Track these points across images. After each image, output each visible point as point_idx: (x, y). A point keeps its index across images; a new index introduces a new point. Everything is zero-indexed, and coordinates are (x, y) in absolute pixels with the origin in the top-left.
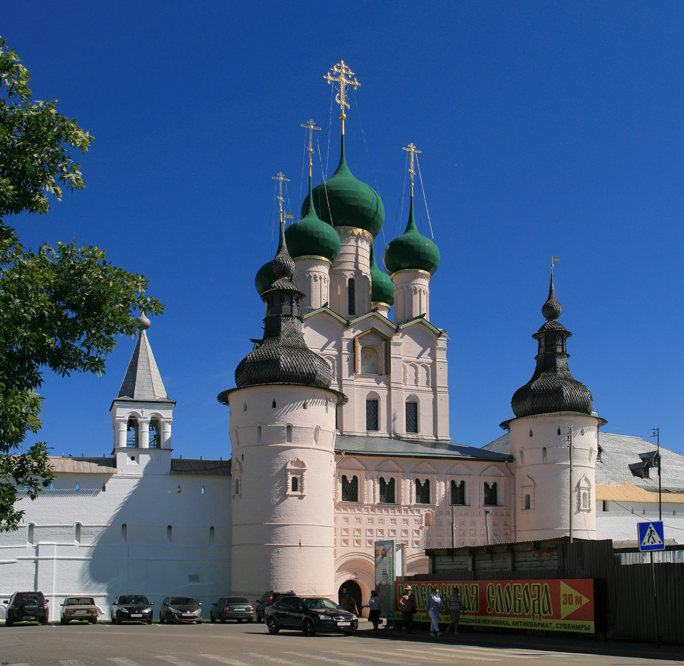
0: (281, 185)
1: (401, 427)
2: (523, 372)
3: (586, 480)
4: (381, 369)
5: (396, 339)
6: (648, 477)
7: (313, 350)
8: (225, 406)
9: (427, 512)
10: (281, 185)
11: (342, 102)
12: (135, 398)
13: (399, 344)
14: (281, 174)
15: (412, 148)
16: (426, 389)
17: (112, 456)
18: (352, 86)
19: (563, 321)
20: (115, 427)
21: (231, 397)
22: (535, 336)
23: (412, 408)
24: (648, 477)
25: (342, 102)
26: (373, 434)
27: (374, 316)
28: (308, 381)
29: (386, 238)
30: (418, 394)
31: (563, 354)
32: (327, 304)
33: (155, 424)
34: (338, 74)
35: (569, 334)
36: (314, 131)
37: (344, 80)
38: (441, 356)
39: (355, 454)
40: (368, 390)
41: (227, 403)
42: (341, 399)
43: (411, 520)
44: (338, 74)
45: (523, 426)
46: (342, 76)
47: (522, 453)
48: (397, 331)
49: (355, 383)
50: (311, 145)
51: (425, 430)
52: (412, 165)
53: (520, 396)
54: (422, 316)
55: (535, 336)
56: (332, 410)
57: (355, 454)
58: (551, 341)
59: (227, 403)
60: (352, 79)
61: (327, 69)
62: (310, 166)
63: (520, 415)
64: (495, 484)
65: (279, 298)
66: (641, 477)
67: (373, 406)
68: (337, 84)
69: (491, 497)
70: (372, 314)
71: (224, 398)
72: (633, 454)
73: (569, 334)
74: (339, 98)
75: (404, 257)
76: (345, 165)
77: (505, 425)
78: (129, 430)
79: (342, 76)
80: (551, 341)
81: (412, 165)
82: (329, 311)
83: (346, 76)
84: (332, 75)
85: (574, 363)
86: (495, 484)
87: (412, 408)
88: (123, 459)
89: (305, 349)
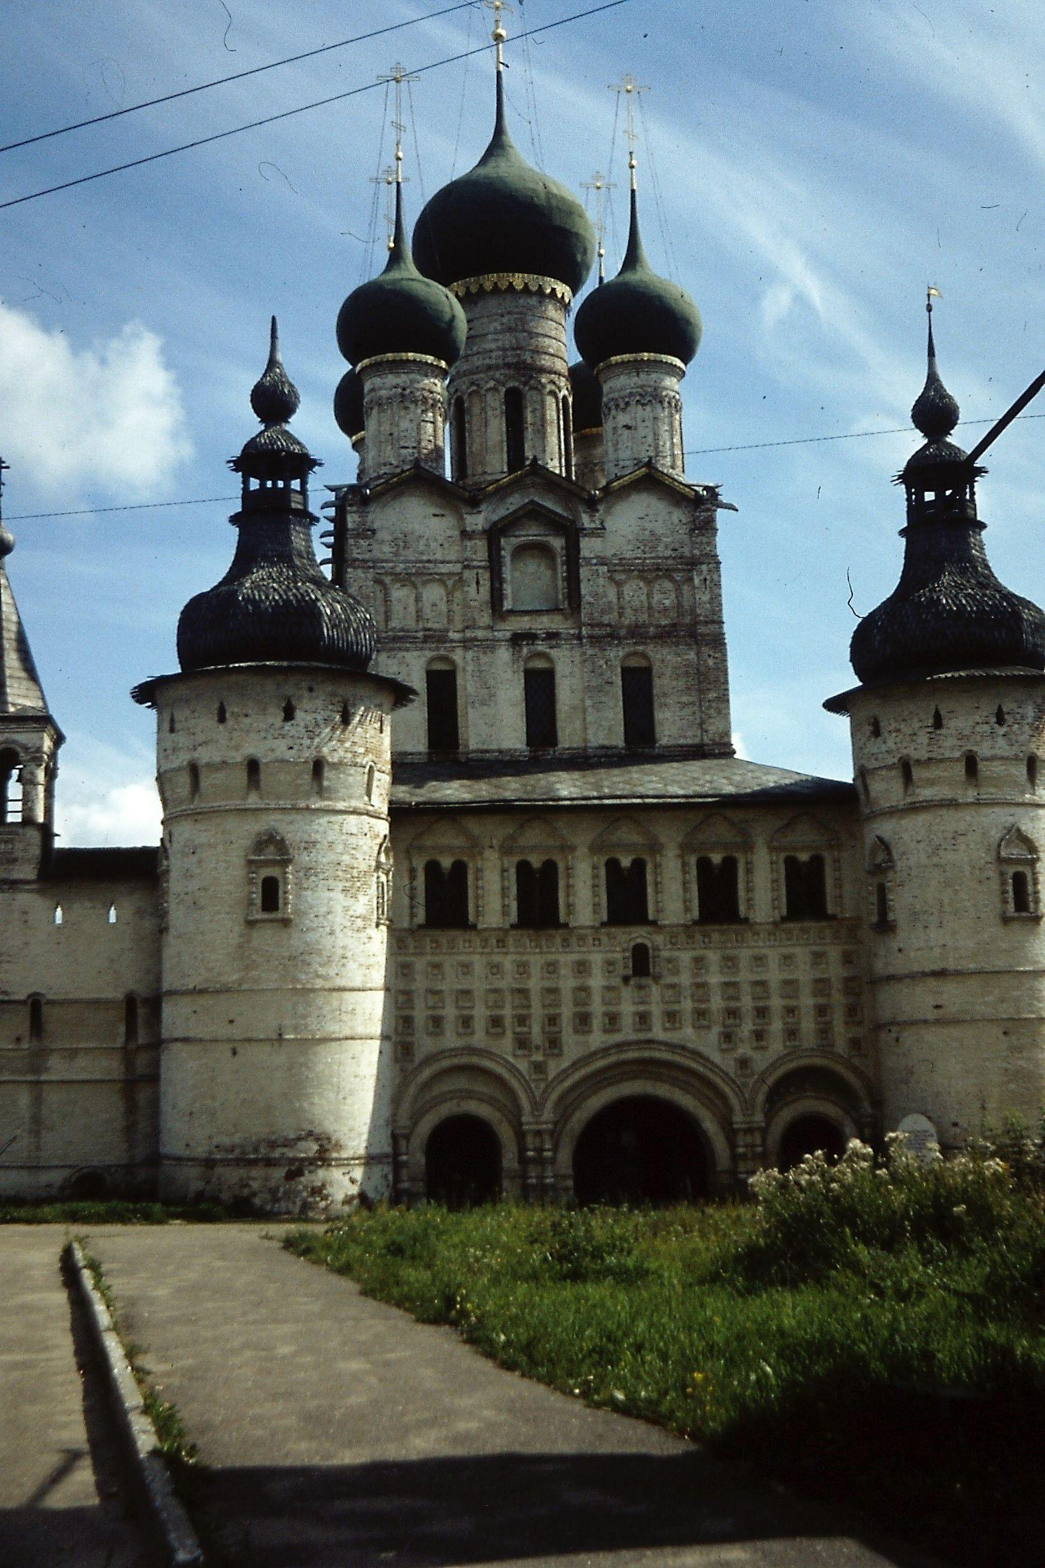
9: (639, 941)
43: (597, 959)
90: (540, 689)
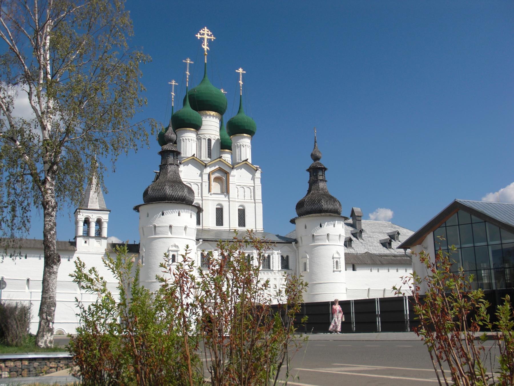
0: (188, 66)
1: (235, 224)
2: (301, 192)
3: (338, 253)
4: (226, 191)
5: (234, 172)
6: (391, 248)
7: (184, 183)
8: (137, 213)
10: (188, 66)
11: (205, 47)
12: (89, 208)
13: (234, 176)
14: (174, 81)
15: (241, 70)
16: (250, 201)
17: (74, 241)
18: (211, 39)
19: (323, 162)
20: (77, 223)
21: (140, 209)
22: (308, 170)
23: (242, 214)
24: (391, 248)
25: (205, 47)
26: (220, 228)
27: (220, 160)
28: (184, 200)
29: (227, 117)
30: (245, 204)
31: (324, 181)
32: (194, 155)
33: (99, 222)
34: (203, 34)
35: (325, 169)
36: (190, 64)
37: (206, 37)
38: (258, 182)
39: (207, 241)
40: (217, 203)
41: (138, 211)
42: (199, 210)
44: (203, 34)
45: (302, 222)
46: (205, 34)
47: (301, 238)
48: (233, 168)
49: (210, 199)
50: (188, 70)
51: (250, 225)
52: (241, 79)
53: (300, 205)
54: (246, 160)
55: (308, 170)
56: (194, 217)
57: (207, 241)
58: (316, 172)
59: (138, 211)
60: (211, 36)
61: (197, 32)
62: (205, 55)
63: (300, 215)
64: (287, 257)
65: (170, 153)
66: (386, 248)
67: (220, 212)
68: (203, 39)
69: (285, 263)
70: (219, 159)
71: (137, 209)
72: (384, 233)
73: (325, 169)
74: (204, 45)
75: (234, 128)
76: (207, 78)
77: (293, 221)
78: (84, 225)
79: (205, 34)
80: (316, 172)
81: (241, 79)
82: (196, 159)
83: (208, 35)
84: (200, 34)
85: (329, 185)
86: (287, 257)
87: (242, 214)
88: (80, 242)
89: (180, 182)
90: (220, 212)
